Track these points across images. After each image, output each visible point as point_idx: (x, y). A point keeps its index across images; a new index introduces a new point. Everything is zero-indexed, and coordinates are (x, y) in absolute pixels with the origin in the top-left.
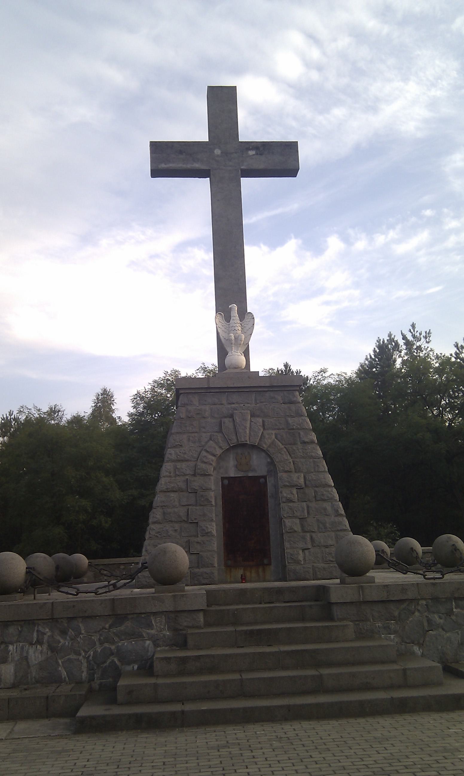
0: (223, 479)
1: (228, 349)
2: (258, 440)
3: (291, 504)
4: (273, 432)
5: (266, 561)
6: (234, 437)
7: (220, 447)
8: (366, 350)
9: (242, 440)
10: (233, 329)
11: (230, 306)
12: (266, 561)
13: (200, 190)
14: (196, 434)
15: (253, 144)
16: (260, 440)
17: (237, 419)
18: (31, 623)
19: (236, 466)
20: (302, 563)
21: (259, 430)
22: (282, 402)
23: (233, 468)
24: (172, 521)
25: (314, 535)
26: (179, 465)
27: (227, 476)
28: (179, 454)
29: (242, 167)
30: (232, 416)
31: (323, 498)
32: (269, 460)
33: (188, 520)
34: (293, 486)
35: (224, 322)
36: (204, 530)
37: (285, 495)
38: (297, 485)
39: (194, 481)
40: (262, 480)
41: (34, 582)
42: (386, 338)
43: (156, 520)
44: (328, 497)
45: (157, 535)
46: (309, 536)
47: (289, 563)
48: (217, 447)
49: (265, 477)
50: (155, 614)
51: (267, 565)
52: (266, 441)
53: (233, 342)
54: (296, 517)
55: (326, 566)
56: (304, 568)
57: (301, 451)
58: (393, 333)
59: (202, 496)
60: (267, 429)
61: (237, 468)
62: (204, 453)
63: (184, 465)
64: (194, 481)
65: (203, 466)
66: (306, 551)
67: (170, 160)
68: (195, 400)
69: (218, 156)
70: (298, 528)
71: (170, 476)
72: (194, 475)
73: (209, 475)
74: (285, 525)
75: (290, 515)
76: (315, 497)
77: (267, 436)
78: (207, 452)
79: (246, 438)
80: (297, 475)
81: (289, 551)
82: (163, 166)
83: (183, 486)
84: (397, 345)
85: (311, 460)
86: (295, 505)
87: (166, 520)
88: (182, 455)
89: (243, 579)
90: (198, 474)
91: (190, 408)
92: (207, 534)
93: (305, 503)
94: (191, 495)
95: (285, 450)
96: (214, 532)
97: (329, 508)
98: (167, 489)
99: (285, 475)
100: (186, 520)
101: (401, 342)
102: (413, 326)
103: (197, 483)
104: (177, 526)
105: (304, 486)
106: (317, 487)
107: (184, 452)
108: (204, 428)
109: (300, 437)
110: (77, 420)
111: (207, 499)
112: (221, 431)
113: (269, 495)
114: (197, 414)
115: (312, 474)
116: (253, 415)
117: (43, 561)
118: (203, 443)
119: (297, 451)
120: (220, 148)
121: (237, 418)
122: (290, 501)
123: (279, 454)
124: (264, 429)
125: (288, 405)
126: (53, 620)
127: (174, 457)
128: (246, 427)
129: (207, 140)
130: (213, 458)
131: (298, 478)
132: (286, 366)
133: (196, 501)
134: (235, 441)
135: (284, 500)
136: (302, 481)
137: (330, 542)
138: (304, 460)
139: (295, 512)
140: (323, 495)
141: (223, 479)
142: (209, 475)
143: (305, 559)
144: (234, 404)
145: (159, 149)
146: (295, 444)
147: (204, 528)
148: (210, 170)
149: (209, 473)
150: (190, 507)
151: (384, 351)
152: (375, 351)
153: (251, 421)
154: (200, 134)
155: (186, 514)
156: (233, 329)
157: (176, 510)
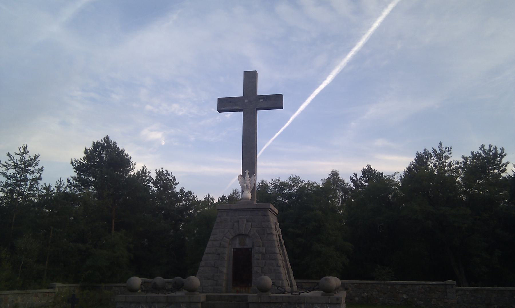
30: (238, 222)
50: (182, 303)
58: (427, 149)
62: (225, 238)
67: (225, 105)
82: (223, 109)
84: (431, 156)
89: (237, 292)
101: (433, 154)
102: (441, 144)
116: (247, 221)
129: (242, 95)
132: (369, 166)
136: (264, 251)
145: (220, 101)
151: (421, 160)
152: (415, 160)
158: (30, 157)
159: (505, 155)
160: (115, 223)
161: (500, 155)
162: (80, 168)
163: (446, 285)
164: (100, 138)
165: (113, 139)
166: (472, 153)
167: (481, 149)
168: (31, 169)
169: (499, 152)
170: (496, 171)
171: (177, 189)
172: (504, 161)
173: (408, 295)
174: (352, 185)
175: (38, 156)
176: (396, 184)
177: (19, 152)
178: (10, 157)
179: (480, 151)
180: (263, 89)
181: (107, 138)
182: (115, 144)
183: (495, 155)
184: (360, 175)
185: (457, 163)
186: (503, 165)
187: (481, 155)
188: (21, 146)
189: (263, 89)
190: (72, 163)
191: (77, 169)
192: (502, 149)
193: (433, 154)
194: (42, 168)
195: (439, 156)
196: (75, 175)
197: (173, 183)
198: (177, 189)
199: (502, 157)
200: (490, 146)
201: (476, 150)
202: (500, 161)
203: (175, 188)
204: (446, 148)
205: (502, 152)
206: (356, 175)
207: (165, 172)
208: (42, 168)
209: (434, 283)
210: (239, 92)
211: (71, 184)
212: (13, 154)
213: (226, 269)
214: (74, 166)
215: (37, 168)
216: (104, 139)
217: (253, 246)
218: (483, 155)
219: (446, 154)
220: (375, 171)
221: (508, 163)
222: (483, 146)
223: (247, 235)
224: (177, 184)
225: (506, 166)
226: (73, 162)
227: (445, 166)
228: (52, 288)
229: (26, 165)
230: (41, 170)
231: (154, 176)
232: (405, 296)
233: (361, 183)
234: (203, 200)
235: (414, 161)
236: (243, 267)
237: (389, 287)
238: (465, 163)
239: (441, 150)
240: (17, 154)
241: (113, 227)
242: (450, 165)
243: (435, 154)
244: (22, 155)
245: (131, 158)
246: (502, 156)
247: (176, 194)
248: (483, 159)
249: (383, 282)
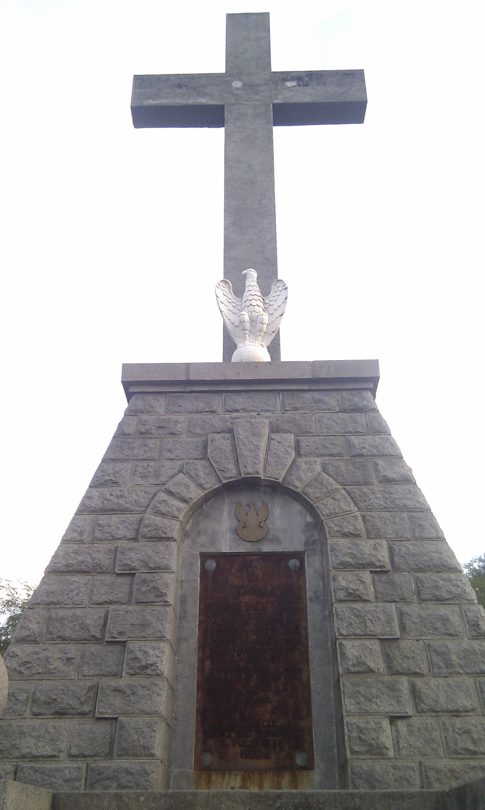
0: (205, 557)
1: (236, 340)
2: (284, 473)
3: (358, 606)
4: (319, 460)
5: (300, 759)
6: (231, 466)
7: (201, 486)
10: (248, 303)
11: (244, 272)
12: (300, 759)
13: (209, 142)
14: (151, 463)
15: (293, 74)
16: (289, 473)
17: (241, 434)
19: (235, 532)
20: (391, 753)
21: (288, 453)
22: (338, 410)
23: (228, 535)
24: (63, 639)
25: (419, 682)
26: (103, 519)
27: (213, 550)
28: (109, 497)
29: (275, 101)
31: (437, 593)
32: (309, 519)
33: (103, 636)
34: (363, 566)
35: (231, 296)
36: (136, 659)
37: (344, 583)
38: (371, 564)
39: (130, 549)
40: (293, 563)
43: (26, 633)
44: (450, 592)
45: (23, 669)
46: (406, 684)
47: (353, 752)
48: (192, 485)
49: (299, 556)
51: (303, 768)
52: (303, 476)
53: (248, 325)
54: (371, 636)
55: (457, 764)
56: (395, 768)
57: (379, 495)
59: (144, 581)
60: (306, 455)
61: (237, 534)
64: (130, 549)
65: (158, 520)
66: (400, 724)
67: (164, 103)
69: (237, 89)
70: (377, 662)
71: (81, 542)
72: (135, 539)
73: (169, 539)
74: (343, 655)
75: (358, 631)
76: (418, 592)
77: (303, 466)
78: (170, 493)
79: (257, 466)
80: (371, 542)
81: (354, 720)
83: (104, 559)
85: (406, 515)
86: (369, 607)
87: (51, 633)
88: (115, 500)
90: (144, 537)
91: (145, 417)
92: (145, 670)
93: (393, 605)
94: (120, 580)
95: (343, 492)
96: (165, 667)
97: (455, 618)
98: (67, 566)
99: (342, 542)
100: (98, 635)
104: (73, 650)
105: (389, 567)
106: (420, 570)
107: (119, 493)
108: (170, 451)
109: (377, 471)
111: (156, 588)
112: (204, 456)
113: (309, 594)
114: (160, 427)
115: (408, 544)
116: (275, 429)
118: (163, 479)
119: (372, 496)
120: (240, 80)
121: (240, 431)
122: (355, 597)
123: (331, 500)
124: (298, 454)
125: (352, 414)
128: (257, 447)
130: (182, 505)
131: (375, 549)
133: (131, 593)
134: (234, 472)
135: (341, 595)
136: (383, 555)
137: (464, 702)
138: (388, 514)
139: (368, 622)
140: (437, 587)
141: (205, 557)
142: (169, 539)
143: (397, 747)
144: (237, 411)
146: (366, 484)
147: (139, 655)
148: (224, 105)
149: (169, 535)
150: (112, 607)
153: (270, 439)
155: (101, 622)
156: (248, 303)
157: (78, 612)
180: (287, 55)
189: (287, 55)
223: (277, 489)
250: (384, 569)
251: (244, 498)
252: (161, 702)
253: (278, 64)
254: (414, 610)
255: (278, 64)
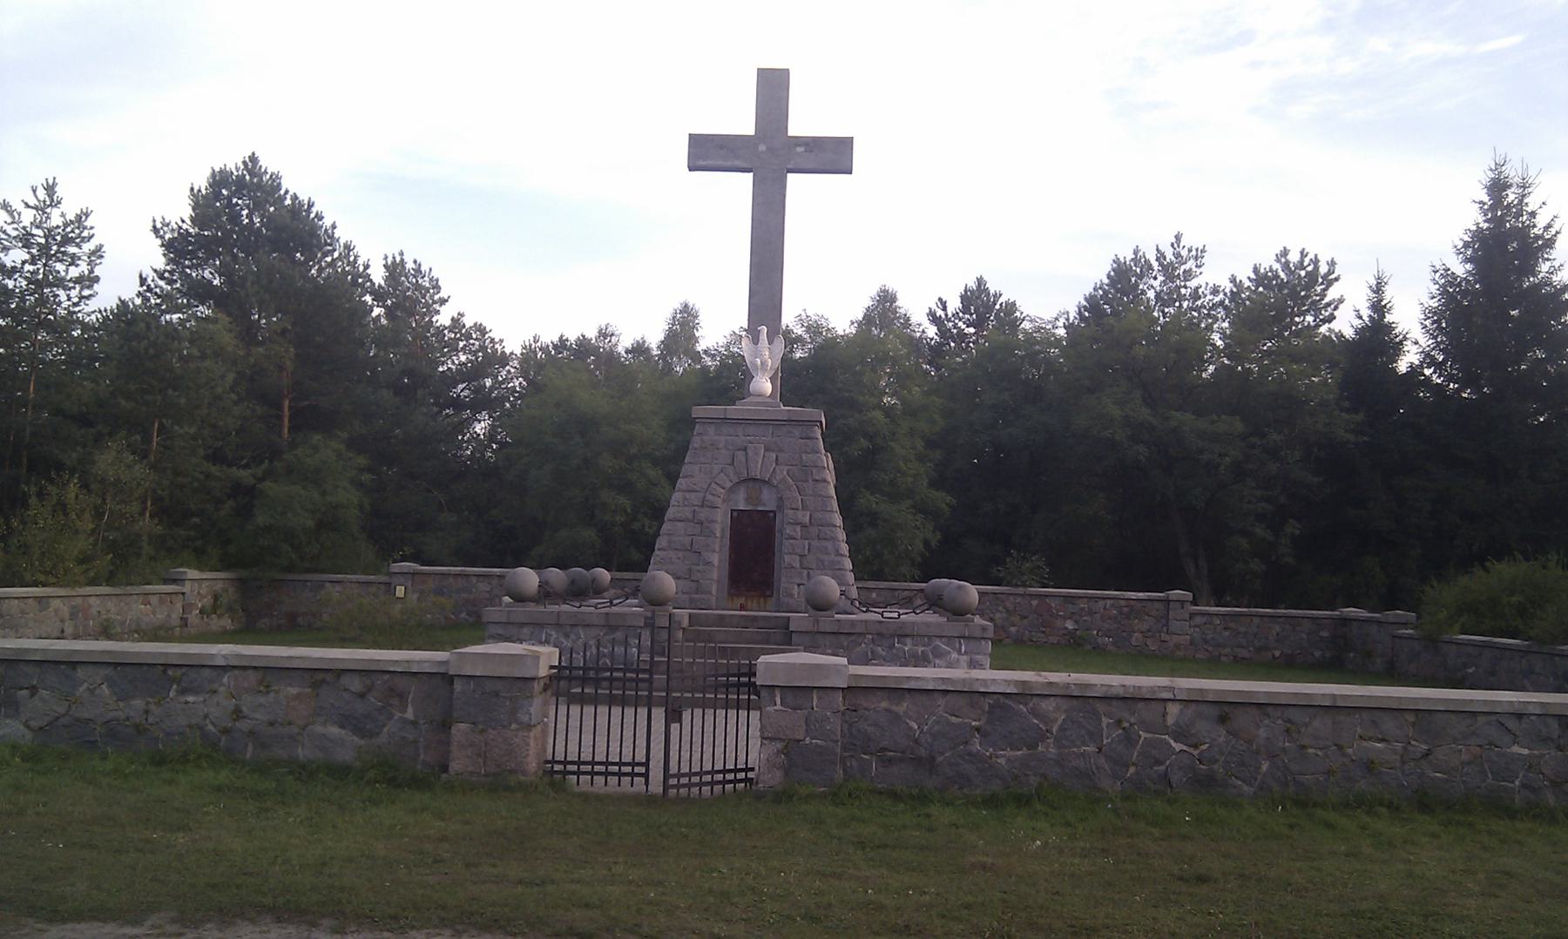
8: (1097, 273)
9: (752, 475)
13: (742, 183)
17: (750, 453)
18: (541, 626)
26: (688, 495)
41: (546, 593)
42: (1130, 256)
58: (1143, 248)
63: (693, 495)
67: (708, 153)
68: (711, 430)
70: (797, 565)
79: (757, 472)
82: (701, 163)
83: (690, 516)
84: (1151, 268)
89: (742, 608)
96: (716, 563)
101: (1155, 265)
102: (1178, 238)
103: (703, 514)
104: (680, 554)
110: (639, 349)
116: (767, 450)
117: (556, 575)
126: (558, 625)
127: (684, 487)
129: (752, 132)
132: (980, 281)
136: (807, 520)
151: (1124, 277)
152: (1109, 276)
154: (747, 127)
158: (63, 215)
159: (1337, 279)
160: (290, 408)
161: (1325, 277)
162: (178, 247)
163: (1167, 601)
164: (232, 161)
165: (268, 164)
166: (1256, 270)
167: (1278, 261)
168: (72, 249)
169: (1323, 269)
170: (1309, 318)
171: (443, 318)
172: (1332, 294)
173: (1076, 622)
174: (932, 331)
175: (87, 215)
176: (1059, 340)
177: (33, 202)
178: (11, 213)
179: (1276, 266)
180: (802, 122)
181: (253, 158)
182: (276, 178)
183: (1313, 277)
184: (954, 304)
185: (1215, 291)
186: (1328, 305)
187: (1277, 277)
188: (39, 182)
189: (802, 122)
190: (155, 230)
191: (168, 246)
192: (1332, 264)
193: (1155, 265)
194: (99, 248)
195: (1168, 270)
196: (160, 263)
197: (432, 297)
198: (443, 318)
199: (1330, 284)
200: (1303, 254)
201: (1268, 262)
202: (1323, 295)
203: (438, 312)
204: (1190, 251)
205: (1330, 272)
206: (943, 304)
207: (410, 265)
208: (99, 248)
209: (1141, 595)
210: (745, 125)
211: (149, 289)
212: (17, 205)
213: (717, 558)
214: (162, 237)
215: (88, 247)
216: (244, 163)
217: (780, 507)
218: (1282, 275)
219: (1191, 264)
220: (997, 296)
221: (1341, 301)
222: (1285, 252)
223: (767, 483)
224: (443, 301)
225: (1336, 308)
226: (159, 225)
227: (1181, 298)
228: (174, 581)
229: (59, 242)
230: (97, 253)
231: (378, 275)
232: (1070, 625)
233: (955, 326)
234: (518, 351)
235: (1106, 281)
236: (754, 554)
237: (1035, 603)
238: (1234, 296)
239: (1178, 255)
240: (27, 206)
241: (286, 420)
242: (1196, 295)
243: (1161, 264)
244: (41, 209)
245: (334, 227)
246: (1329, 281)
247: (440, 331)
248: (1282, 285)
249: (1021, 590)
250: (734, 410)
251: (751, 484)
252: (715, 576)
253: (794, 130)
254: (815, 543)
255: (794, 130)
